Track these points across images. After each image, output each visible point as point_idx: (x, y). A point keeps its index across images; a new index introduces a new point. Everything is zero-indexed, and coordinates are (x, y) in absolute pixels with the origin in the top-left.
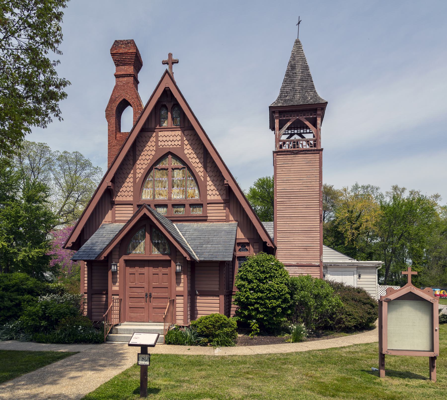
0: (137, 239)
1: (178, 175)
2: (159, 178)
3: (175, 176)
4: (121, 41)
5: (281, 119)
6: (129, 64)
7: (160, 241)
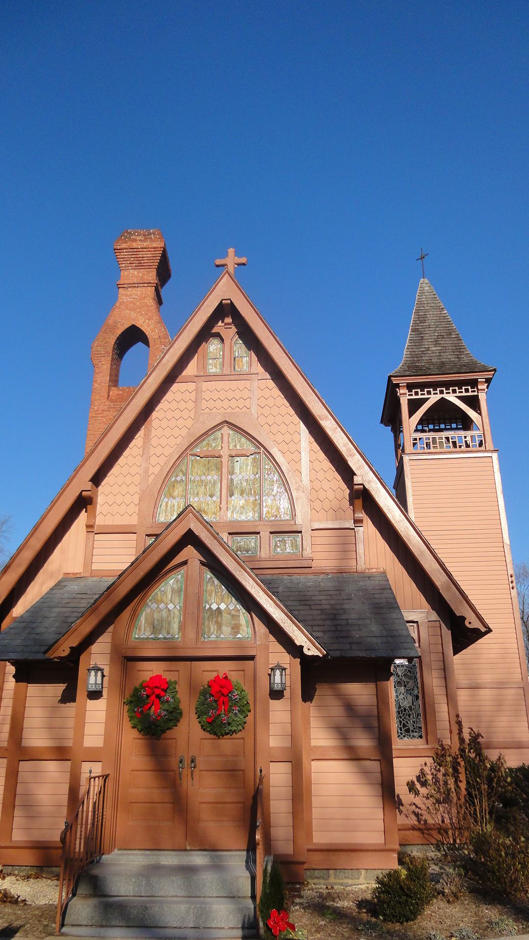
1: (244, 470)
2: (200, 476)
3: (237, 470)
6: (150, 267)
7: (223, 606)
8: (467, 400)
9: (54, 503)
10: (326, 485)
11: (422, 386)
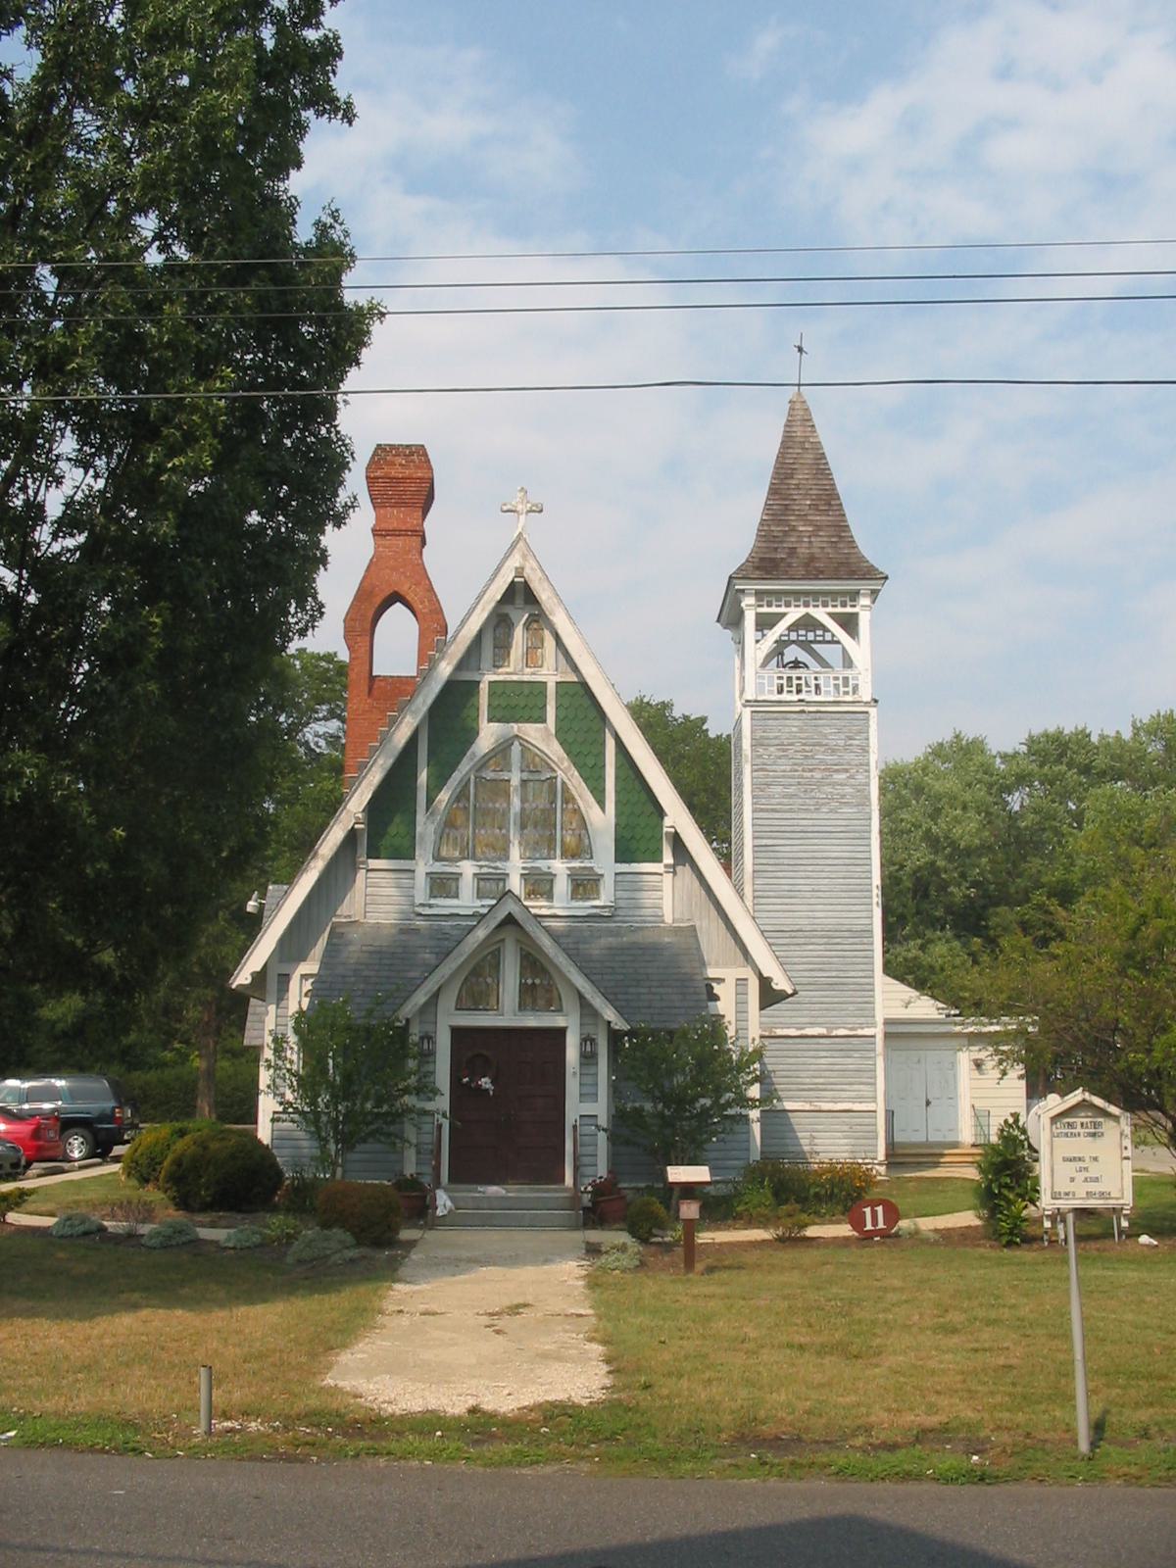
0: (480, 976)
4: (392, 447)
5: (760, 610)
7: (537, 981)
8: (839, 618)
9: (480, 598)
10: (305, 1144)
11: (778, 594)
